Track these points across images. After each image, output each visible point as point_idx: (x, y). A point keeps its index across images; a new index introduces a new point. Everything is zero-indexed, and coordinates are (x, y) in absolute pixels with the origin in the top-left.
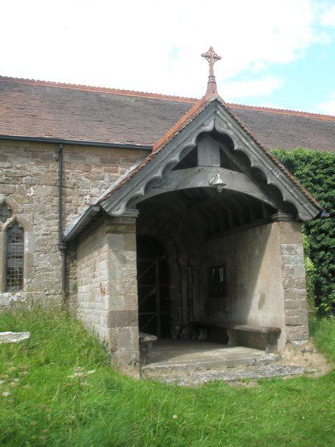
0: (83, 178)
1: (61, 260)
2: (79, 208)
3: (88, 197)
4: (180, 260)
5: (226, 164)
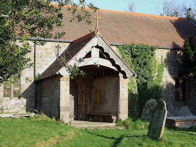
0: (44, 54)
1: (35, 87)
2: (43, 66)
3: (46, 61)
4: (83, 88)
5: (101, 56)
